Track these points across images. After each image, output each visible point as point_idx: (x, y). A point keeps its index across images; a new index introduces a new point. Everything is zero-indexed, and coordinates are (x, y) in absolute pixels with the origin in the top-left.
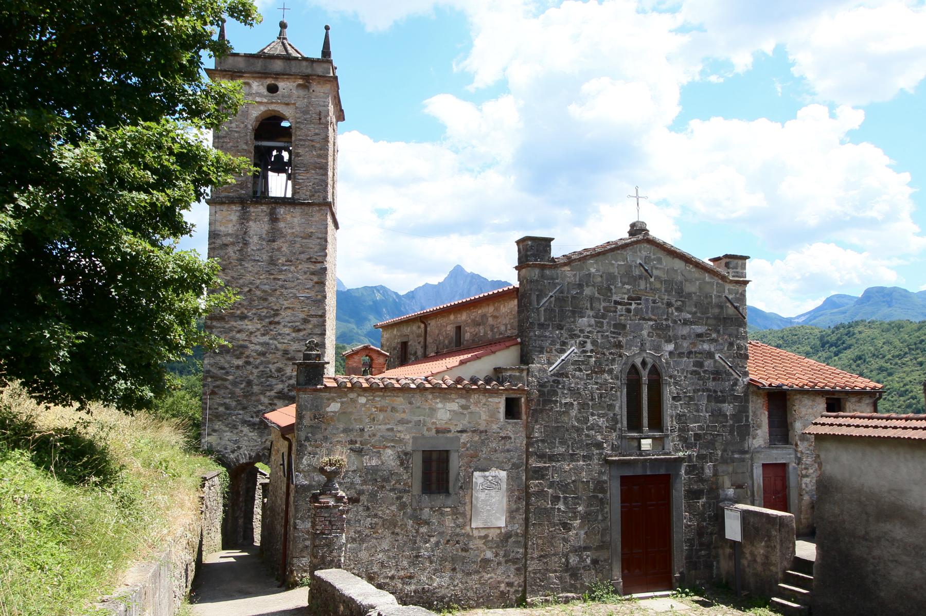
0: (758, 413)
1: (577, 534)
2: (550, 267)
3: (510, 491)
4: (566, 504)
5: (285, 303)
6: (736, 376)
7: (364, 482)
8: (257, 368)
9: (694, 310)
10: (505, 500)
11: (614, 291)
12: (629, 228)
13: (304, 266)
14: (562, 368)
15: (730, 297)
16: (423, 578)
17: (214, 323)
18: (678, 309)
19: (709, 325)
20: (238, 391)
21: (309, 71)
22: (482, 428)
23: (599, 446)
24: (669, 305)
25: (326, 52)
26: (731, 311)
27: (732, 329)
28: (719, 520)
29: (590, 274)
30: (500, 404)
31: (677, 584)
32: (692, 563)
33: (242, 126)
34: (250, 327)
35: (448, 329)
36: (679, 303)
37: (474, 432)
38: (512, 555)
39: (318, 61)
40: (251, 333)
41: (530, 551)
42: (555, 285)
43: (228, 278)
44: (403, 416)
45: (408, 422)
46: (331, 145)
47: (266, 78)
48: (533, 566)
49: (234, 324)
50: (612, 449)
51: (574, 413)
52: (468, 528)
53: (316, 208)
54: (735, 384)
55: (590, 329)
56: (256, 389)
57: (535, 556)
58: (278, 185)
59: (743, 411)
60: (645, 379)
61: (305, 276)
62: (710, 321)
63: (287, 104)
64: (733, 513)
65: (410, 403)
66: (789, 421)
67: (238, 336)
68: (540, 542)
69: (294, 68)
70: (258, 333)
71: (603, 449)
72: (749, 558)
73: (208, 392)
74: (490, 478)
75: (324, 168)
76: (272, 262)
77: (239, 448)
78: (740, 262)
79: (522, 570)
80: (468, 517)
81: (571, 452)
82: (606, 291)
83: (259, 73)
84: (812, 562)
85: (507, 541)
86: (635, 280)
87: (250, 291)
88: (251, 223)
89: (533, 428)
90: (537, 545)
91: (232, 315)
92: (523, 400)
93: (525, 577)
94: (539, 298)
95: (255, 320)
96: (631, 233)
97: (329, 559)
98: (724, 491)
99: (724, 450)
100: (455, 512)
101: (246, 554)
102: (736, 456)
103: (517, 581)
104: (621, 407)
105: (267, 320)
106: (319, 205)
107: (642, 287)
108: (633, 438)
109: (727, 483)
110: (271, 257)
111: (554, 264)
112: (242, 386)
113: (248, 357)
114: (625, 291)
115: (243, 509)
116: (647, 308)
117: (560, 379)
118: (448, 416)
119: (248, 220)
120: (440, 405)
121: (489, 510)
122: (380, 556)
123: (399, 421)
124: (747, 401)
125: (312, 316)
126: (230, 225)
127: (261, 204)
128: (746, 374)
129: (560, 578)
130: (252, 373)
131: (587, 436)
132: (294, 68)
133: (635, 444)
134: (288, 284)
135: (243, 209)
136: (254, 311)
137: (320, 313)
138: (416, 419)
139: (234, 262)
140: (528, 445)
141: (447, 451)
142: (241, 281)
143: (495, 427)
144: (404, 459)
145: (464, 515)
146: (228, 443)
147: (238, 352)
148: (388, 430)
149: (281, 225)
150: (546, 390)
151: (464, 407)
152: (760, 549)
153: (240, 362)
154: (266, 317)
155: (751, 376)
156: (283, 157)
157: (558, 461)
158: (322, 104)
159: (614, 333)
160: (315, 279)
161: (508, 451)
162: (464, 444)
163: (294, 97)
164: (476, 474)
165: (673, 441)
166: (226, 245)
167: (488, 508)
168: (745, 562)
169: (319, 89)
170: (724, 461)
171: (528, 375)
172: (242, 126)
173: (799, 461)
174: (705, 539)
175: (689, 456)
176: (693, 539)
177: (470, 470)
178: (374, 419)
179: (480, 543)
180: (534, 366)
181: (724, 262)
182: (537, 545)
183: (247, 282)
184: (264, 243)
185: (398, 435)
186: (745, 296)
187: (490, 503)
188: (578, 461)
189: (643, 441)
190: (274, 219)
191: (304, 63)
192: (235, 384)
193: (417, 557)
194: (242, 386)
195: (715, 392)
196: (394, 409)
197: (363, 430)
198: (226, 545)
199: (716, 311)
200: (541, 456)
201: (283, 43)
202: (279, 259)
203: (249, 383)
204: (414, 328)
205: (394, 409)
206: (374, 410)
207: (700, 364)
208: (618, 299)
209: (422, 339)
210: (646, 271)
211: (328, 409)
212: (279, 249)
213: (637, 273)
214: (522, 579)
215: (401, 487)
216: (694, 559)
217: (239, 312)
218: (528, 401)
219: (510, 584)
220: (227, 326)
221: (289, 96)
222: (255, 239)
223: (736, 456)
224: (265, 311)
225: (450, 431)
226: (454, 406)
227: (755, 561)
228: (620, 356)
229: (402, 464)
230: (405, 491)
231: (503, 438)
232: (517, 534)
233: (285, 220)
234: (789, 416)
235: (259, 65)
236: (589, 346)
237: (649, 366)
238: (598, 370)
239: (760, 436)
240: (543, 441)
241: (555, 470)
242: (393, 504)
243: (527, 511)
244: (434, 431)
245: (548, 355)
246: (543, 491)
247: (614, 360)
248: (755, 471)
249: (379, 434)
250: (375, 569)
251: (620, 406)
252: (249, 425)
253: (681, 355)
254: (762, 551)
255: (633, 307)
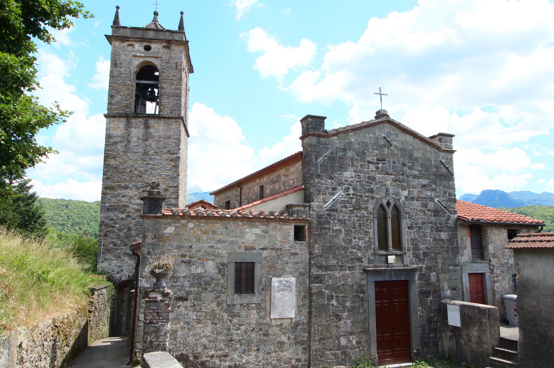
0: (464, 238)
1: (345, 323)
2: (324, 137)
3: (298, 292)
4: (337, 301)
5: (153, 178)
6: (449, 214)
7: (192, 285)
8: (135, 219)
9: (420, 169)
10: (294, 299)
11: (367, 155)
12: (375, 115)
13: (165, 156)
14: (333, 205)
15: (443, 161)
16: (235, 356)
17: (108, 191)
18: (410, 168)
19: (430, 180)
20: (122, 234)
21: (170, 38)
22: (278, 247)
23: (360, 260)
24: (404, 165)
25: (181, 26)
26: (444, 170)
27: (445, 183)
28: (442, 311)
29: (351, 143)
30: (290, 229)
31: (415, 358)
32: (425, 343)
33: (128, 70)
34: (130, 194)
35: (255, 188)
36: (410, 164)
37: (272, 249)
38: (300, 338)
39: (176, 32)
40: (131, 197)
41: (312, 335)
42: (328, 149)
43: (117, 163)
44: (221, 237)
45: (224, 242)
46: (184, 86)
47: (143, 41)
48: (315, 346)
49: (121, 192)
50: (369, 262)
51: (342, 236)
52: (268, 319)
53: (173, 120)
54: (449, 219)
55: (352, 179)
56: (133, 233)
57: (317, 339)
58: (151, 108)
59: (453, 238)
60: (389, 215)
61: (166, 162)
62: (431, 177)
63: (157, 58)
64: (454, 307)
65: (226, 228)
66: (484, 245)
67: (123, 199)
68: (320, 328)
69: (161, 36)
70: (135, 198)
71: (362, 262)
72: (466, 339)
73: (103, 234)
74: (284, 282)
75: (179, 96)
76: (145, 153)
77: (122, 271)
78: (448, 138)
79: (307, 349)
80: (268, 310)
81: (340, 264)
82: (362, 154)
83: (139, 38)
84: (516, 342)
85: (296, 329)
86: (381, 148)
87: (131, 171)
88: (133, 129)
89: (314, 247)
90: (318, 331)
91: (120, 186)
92: (306, 227)
93: (310, 354)
94: (317, 157)
95: (134, 189)
96: (376, 117)
97: (156, 343)
98: (444, 292)
99: (443, 264)
100: (259, 307)
101: (120, 340)
102: (451, 268)
103: (303, 357)
104: (374, 233)
105: (141, 189)
106: (175, 118)
107: (386, 152)
108: (382, 255)
109: (446, 286)
110: (145, 150)
111: (327, 135)
112: (125, 231)
113: (129, 212)
114: (375, 155)
115: (126, 311)
116: (390, 166)
117: (332, 213)
118: (254, 237)
119: (130, 127)
120: (248, 230)
121: (283, 306)
122: (203, 340)
123: (218, 241)
124: (456, 231)
125: (170, 187)
126: (119, 130)
127: (139, 117)
128: (455, 212)
129: (335, 355)
130: (131, 223)
131: (351, 252)
132: (161, 36)
133: (383, 259)
134: (155, 167)
135: (127, 120)
136: (133, 183)
137: (175, 185)
138: (231, 239)
139: (121, 153)
140: (310, 259)
141: (253, 263)
142: (125, 165)
143: (287, 246)
144: (221, 268)
145: (265, 309)
146: (115, 267)
147: (122, 210)
148: (210, 247)
149: (152, 130)
150: (322, 220)
151: (265, 232)
152: (474, 332)
153: (124, 216)
154: (141, 187)
155: (459, 215)
156: (155, 92)
157: (332, 270)
158: (178, 57)
159: (368, 182)
160: (173, 164)
161: (296, 263)
162: (266, 258)
163: (161, 53)
164: (274, 279)
165: (409, 257)
166: (117, 143)
167: (283, 304)
168: (462, 342)
169: (177, 49)
170: (444, 271)
171: (310, 210)
172: (128, 70)
173: (492, 271)
174: (433, 326)
175: (421, 267)
176: (425, 326)
177: (270, 277)
178: (199, 239)
179: (277, 330)
180: (314, 204)
181: (437, 138)
182: (318, 331)
183: (129, 166)
184: (140, 141)
185: (217, 251)
186: (452, 161)
187: (284, 300)
188: (345, 270)
189: (389, 257)
190: (147, 127)
191: (168, 33)
192: (120, 230)
193: (231, 340)
194: (125, 231)
195: (436, 224)
196: (214, 232)
197: (191, 247)
198: (112, 333)
199: (434, 170)
200: (320, 267)
201: (155, 24)
202: (150, 151)
203: (129, 229)
204: (234, 192)
205: (214, 232)
206: (199, 232)
207: (426, 206)
208: (370, 160)
209: (239, 198)
210: (388, 141)
211: (166, 231)
212: (150, 145)
213: (382, 143)
214: (307, 356)
215: (219, 288)
216: (426, 340)
217: (123, 184)
218: (310, 228)
219: (298, 360)
220: (116, 193)
221: (158, 53)
222: (135, 139)
223: (451, 268)
224: (140, 184)
225: (254, 249)
226: (258, 231)
227: (470, 340)
228: (373, 198)
229: (220, 272)
230: (222, 292)
231: (293, 254)
232: (303, 323)
233: (154, 127)
234: (483, 241)
235: (139, 34)
236: (351, 191)
237: (392, 205)
238: (358, 208)
239: (466, 255)
240: (321, 256)
241: (330, 277)
242: (212, 302)
243: (310, 307)
244: (243, 248)
245: (324, 196)
246: (321, 291)
247: (368, 201)
248: (464, 278)
249: (203, 250)
250: (200, 349)
251: (373, 231)
252: (128, 256)
253: (412, 199)
254: (475, 334)
255: (380, 165)
